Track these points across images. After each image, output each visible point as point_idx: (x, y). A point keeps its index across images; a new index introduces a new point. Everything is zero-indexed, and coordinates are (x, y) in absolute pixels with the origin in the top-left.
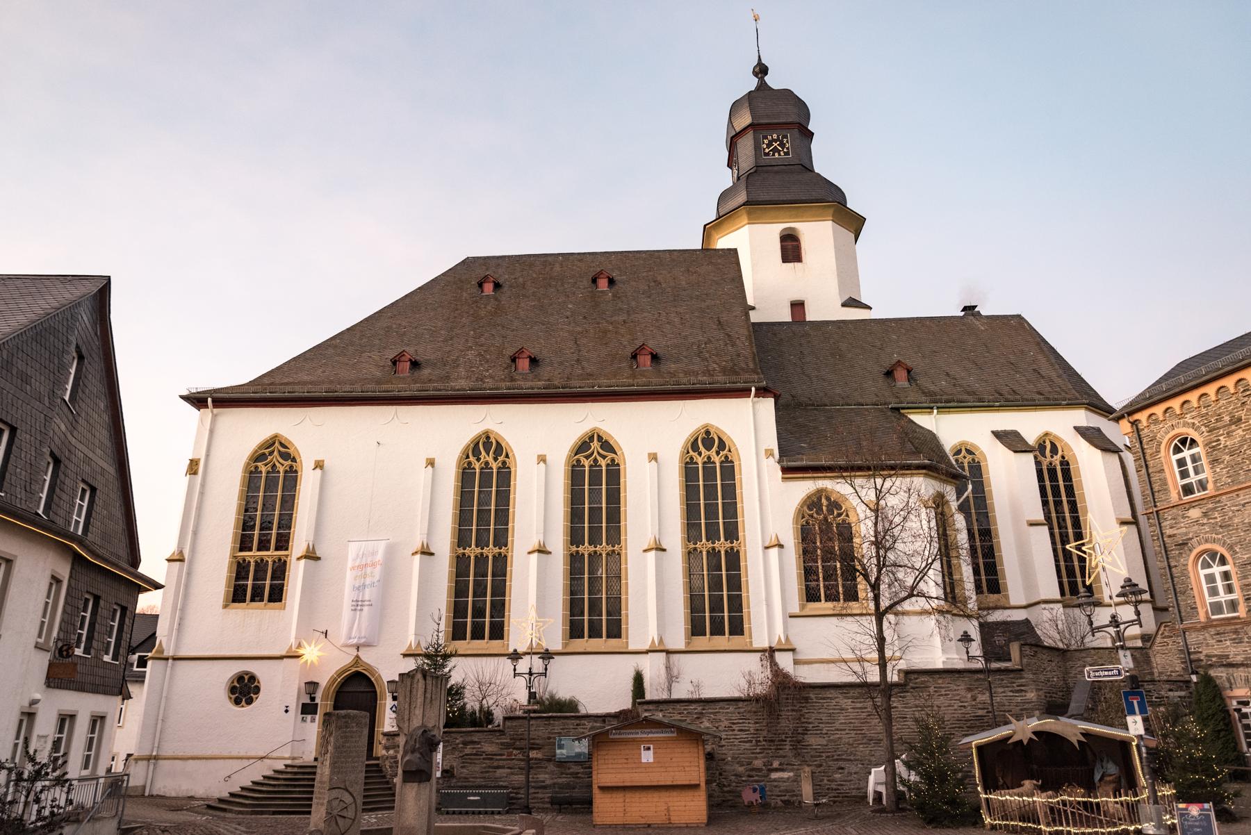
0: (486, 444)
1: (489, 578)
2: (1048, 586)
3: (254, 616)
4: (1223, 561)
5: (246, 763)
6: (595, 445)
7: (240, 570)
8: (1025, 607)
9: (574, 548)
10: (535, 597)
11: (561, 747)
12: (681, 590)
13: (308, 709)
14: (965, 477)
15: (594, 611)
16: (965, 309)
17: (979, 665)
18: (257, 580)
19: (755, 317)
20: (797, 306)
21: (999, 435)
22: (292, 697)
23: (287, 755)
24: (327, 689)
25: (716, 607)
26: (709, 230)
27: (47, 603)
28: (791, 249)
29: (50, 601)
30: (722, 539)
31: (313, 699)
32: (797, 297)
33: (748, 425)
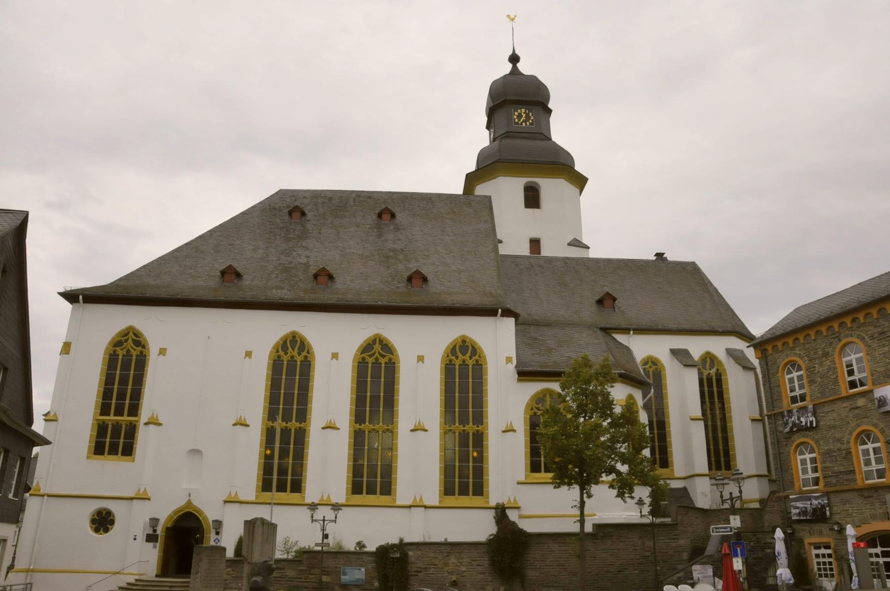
1: (292, 446)
2: (701, 463)
4: (812, 451)
5: (105, 576)
6: (377, 347)
7: (101, 430)
8: (684, 478)
10: (328, 460)
11: (345, 574)
13: (151, 538)
14: (649, 384)
15: (371, 477)
16: (657, 255)
17: (648, 520)
18: (115, 437)
19: (503, 250)
20: (535, 244)
21: (674, 352)
22: (140, 528)
23: (136, 572)
25: (464, 475)
26: (472, 180)
28: (532, 198)
30: (471, 424)
31: (155, 531)
32: (535, 235)
33: (497, 340)
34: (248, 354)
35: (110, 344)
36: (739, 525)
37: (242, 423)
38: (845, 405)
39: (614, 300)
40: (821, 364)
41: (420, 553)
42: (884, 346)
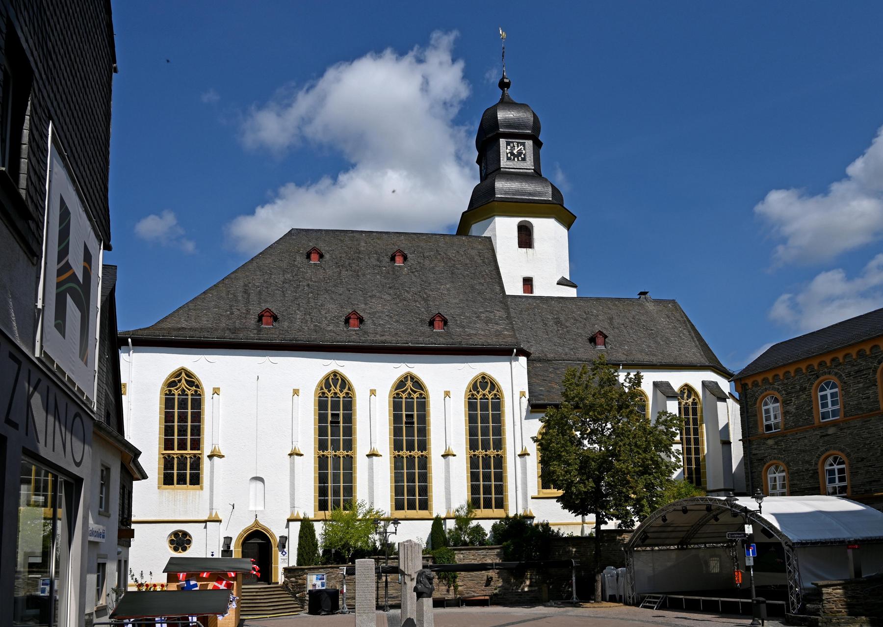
0: (335, 380)
3: (182, 494)
6: (409, 383)
9: (397, 453)
12: (313, 443)
24: (238, 540)
27: (101, 498)
28: (525, 238)
29: (103, 496)
33: (512, 377)
34: (296, 392)
35: (164, 384)
36: (751, 532)
37: (294, 454)
38: (816, 432)
39: (606, 337)
40: (798, 397)
41: (462, 556)
42: (859, 383)
